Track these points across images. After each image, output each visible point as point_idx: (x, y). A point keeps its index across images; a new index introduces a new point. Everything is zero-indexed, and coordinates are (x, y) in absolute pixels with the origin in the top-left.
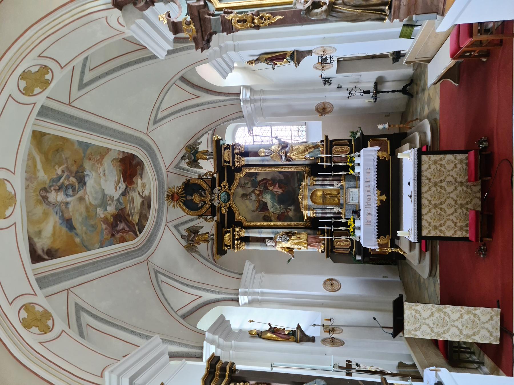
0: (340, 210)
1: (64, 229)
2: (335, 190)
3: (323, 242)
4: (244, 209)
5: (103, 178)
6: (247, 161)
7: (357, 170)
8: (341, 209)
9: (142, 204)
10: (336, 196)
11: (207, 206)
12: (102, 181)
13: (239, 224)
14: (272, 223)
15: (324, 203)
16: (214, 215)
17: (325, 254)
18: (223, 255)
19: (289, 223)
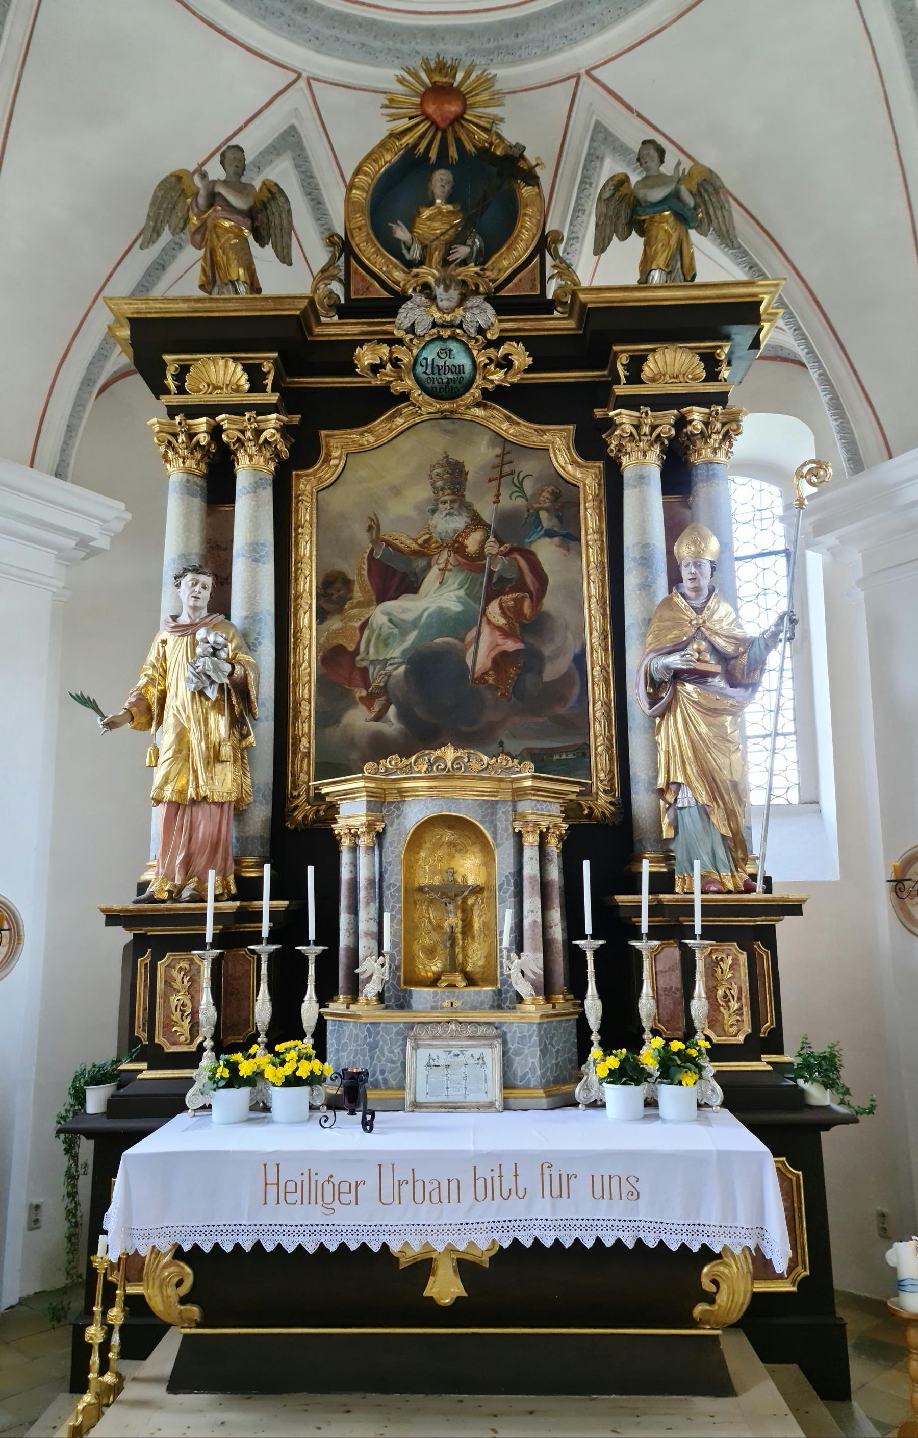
2: (492, 957)
3: (186, 894)
4: (382, 477)
6: (642, 479)
8: (381, 997)
10: (453, 966)
11: (398, 275)
14: (306, 618)
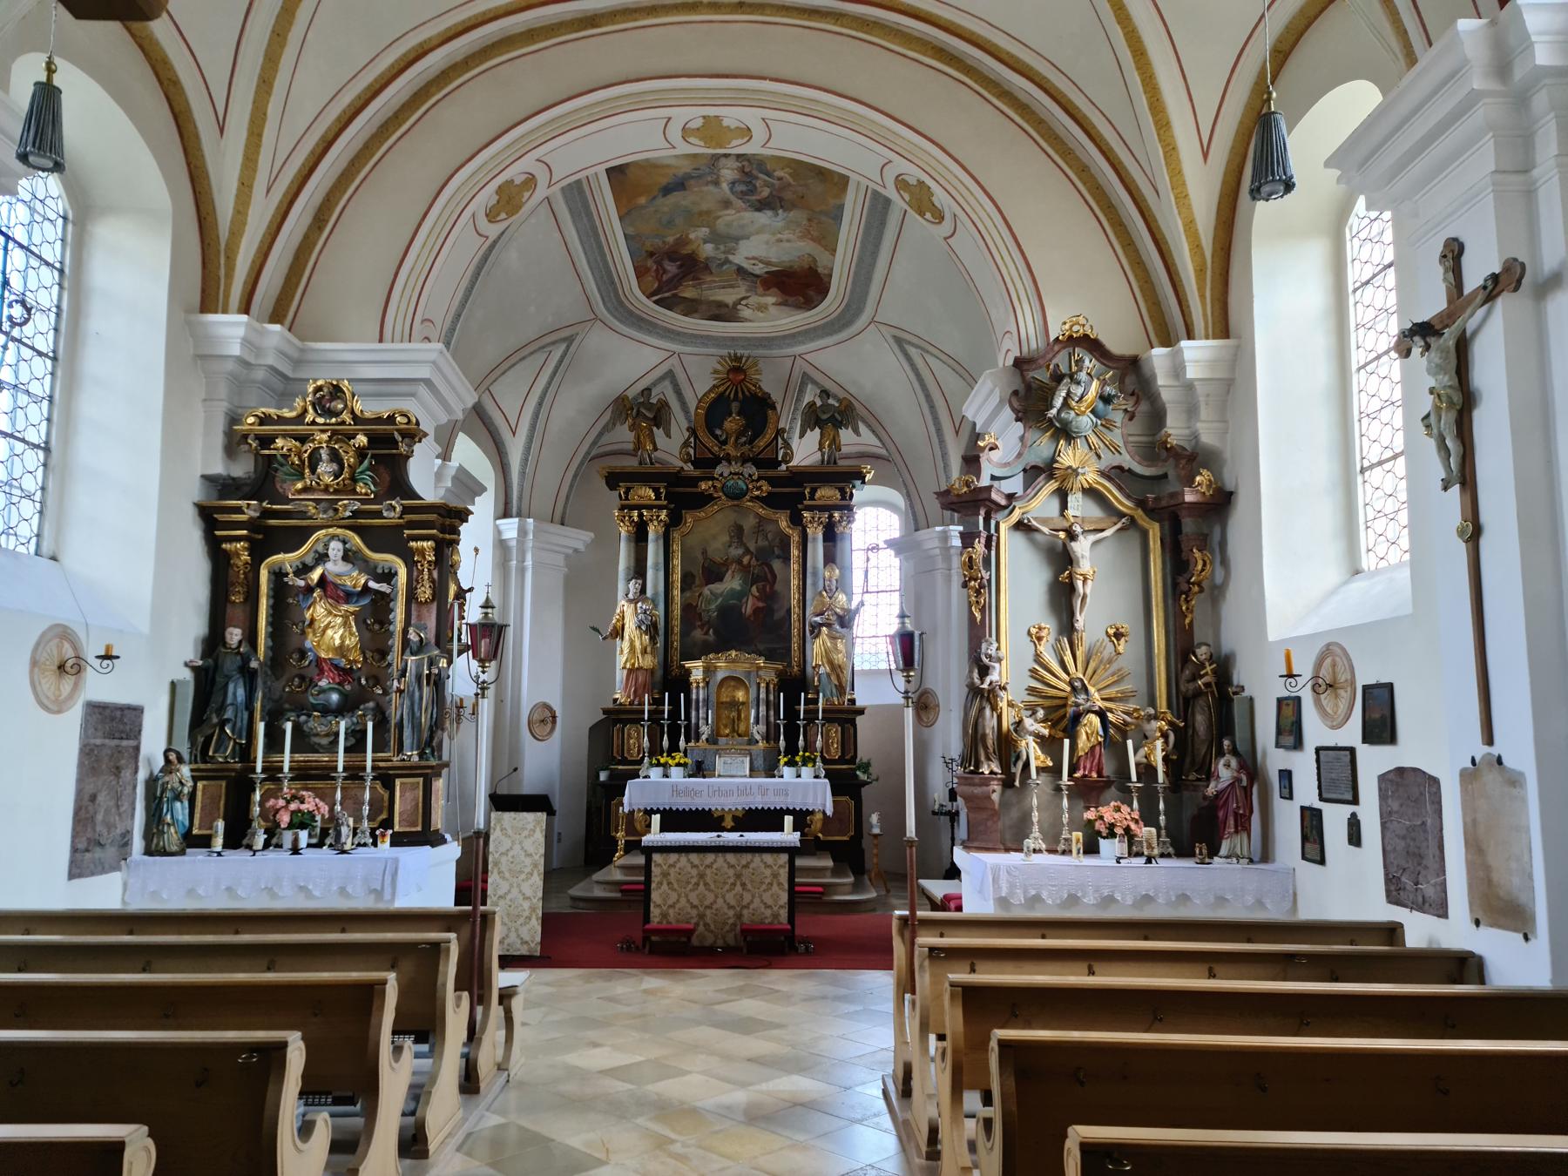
0: (704, 737)
1: (664, 181)
4: (711, 529)
5: (773, 239)
6: (815, 539)
7: (788, 772)
9: (721, 305)
10: (733, 730)
12: (765, 237)
13: (675, 521)
14: (677, 593)
15: (720, 704)
16: (697, 463)
17: (610, 705)
18: (608, 483)
19: (677, 630)
